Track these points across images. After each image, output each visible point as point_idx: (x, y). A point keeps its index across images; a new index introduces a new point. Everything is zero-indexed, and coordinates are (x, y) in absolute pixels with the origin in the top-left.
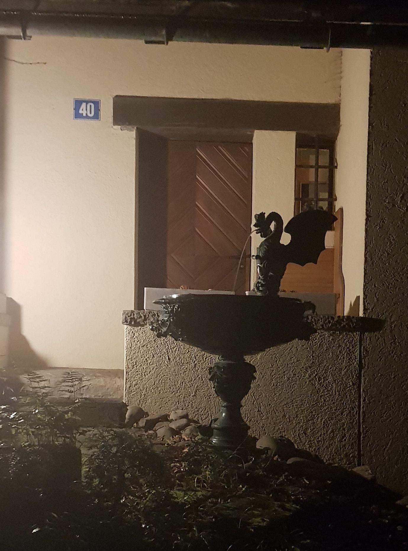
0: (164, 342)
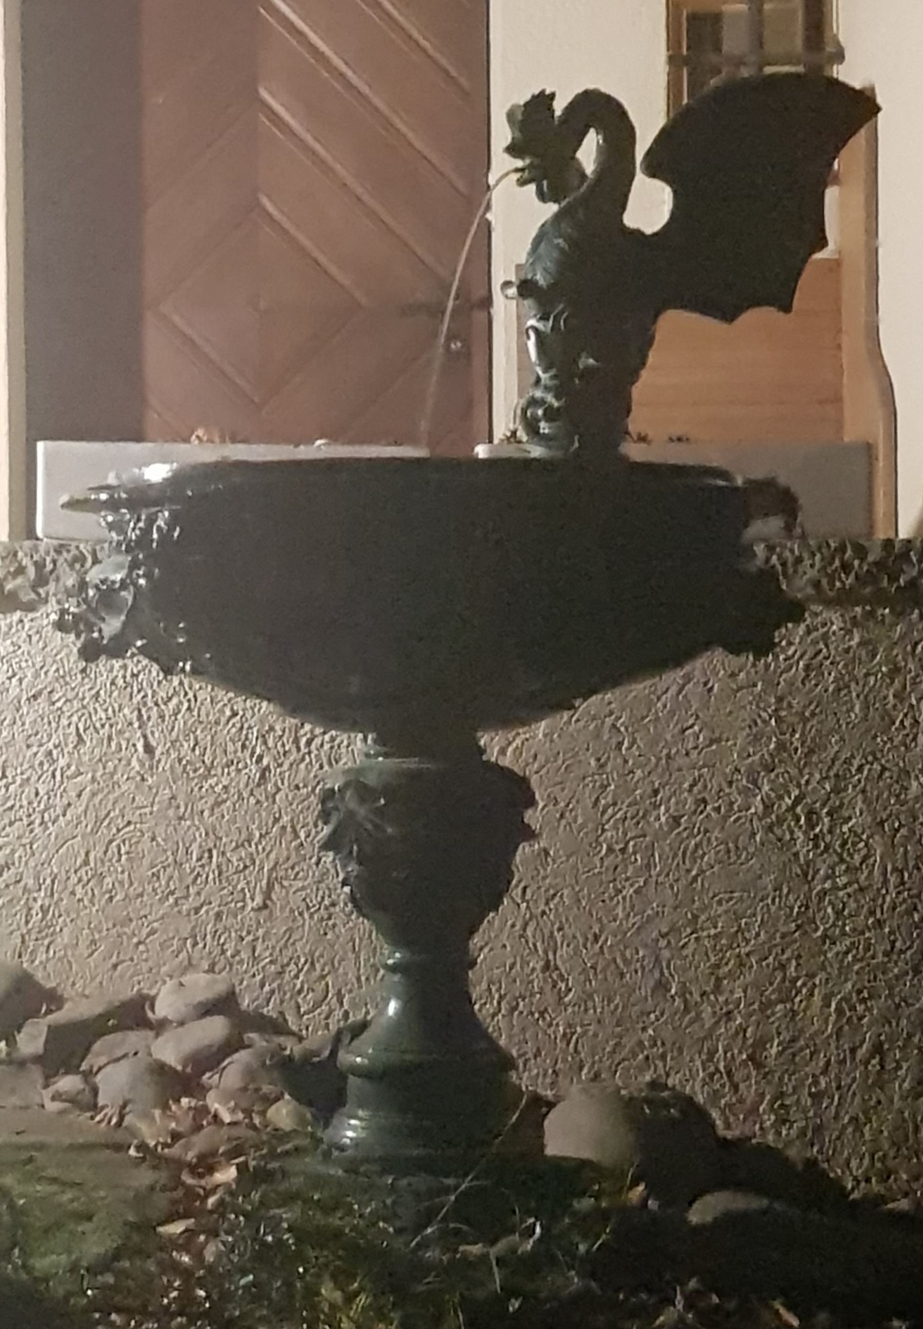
0: (124, 677)
